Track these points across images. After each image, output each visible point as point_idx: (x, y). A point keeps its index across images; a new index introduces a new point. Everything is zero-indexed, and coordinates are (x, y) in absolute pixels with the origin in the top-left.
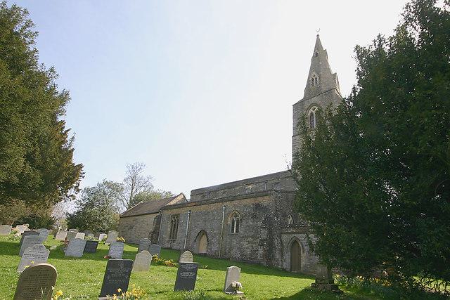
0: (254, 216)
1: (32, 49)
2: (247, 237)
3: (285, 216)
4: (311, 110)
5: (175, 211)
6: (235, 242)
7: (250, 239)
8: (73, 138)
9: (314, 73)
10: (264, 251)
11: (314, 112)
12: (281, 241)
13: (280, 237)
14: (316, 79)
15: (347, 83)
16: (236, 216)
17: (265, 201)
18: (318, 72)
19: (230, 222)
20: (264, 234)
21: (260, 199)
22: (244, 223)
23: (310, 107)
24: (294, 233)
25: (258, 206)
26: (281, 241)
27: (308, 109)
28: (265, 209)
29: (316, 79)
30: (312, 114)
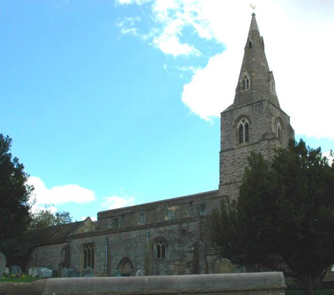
4: (241, 122)
5: (89, 240)
7: (177, 262)
11: (243, 125)
13: (205, 259)
14: (248, 81)
18: (250, 73)
22: (170, 248)
23: (241, 117)
27: (237, 121)
28: (191, 235)
29: (248, 81)
30: (241, 126)
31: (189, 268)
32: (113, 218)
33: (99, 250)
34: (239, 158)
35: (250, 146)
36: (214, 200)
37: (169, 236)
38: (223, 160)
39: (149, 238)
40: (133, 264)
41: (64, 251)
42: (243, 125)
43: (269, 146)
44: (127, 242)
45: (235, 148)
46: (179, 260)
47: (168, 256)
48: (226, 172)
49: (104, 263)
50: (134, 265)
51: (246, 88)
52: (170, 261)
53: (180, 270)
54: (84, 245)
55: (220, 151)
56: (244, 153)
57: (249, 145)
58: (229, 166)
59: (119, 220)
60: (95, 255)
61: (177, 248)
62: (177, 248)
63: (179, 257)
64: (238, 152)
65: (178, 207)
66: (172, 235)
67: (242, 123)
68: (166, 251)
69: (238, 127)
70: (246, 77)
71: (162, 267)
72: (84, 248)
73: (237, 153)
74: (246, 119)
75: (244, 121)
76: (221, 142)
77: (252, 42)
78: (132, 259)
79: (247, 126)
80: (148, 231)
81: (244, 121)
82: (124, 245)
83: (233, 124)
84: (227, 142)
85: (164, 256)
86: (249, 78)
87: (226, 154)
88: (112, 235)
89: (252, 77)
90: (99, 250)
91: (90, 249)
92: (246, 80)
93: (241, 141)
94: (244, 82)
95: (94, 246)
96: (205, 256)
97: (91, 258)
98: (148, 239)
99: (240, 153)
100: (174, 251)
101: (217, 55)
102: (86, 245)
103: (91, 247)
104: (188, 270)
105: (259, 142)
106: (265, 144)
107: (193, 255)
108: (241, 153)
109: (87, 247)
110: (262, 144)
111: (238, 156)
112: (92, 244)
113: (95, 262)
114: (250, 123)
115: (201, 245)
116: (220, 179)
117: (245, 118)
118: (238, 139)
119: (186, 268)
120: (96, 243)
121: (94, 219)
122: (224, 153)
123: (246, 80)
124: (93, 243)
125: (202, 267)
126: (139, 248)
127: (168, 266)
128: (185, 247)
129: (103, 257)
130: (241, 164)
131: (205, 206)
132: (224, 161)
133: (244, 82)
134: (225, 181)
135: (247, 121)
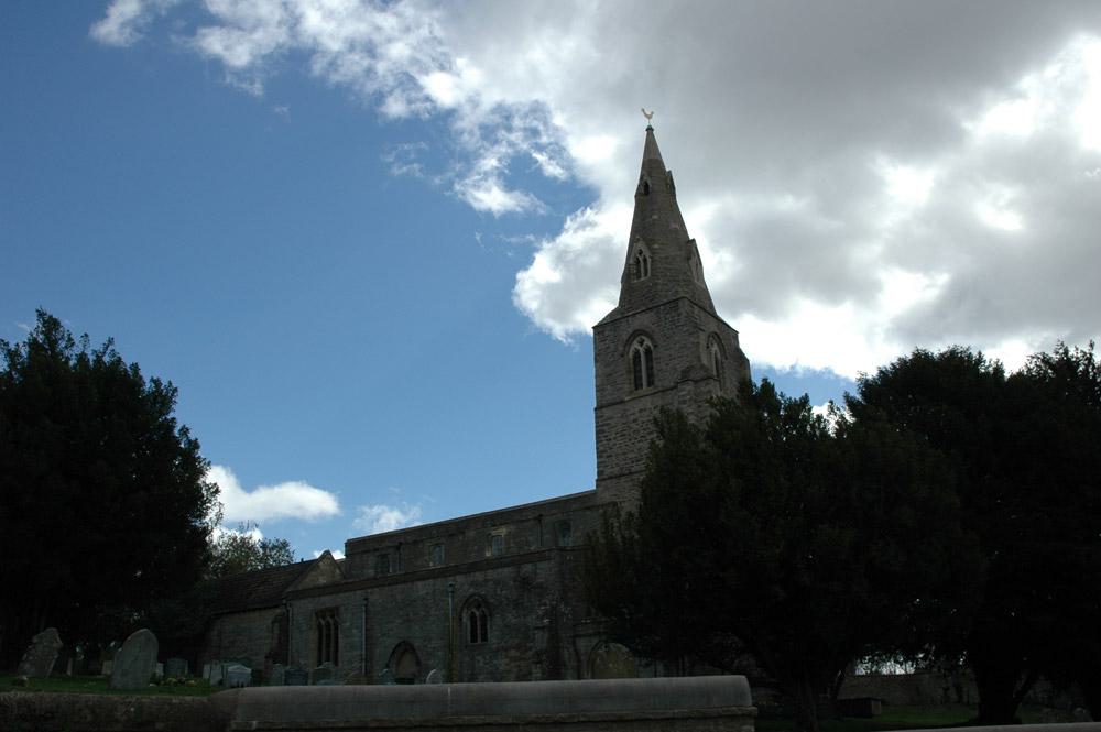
4: (635, 345)
5: (327, 601)
7: (513, 653)
11: (642, 350)
14: (645, 260)
18: (649, 243)
26: (575, 650)
27: (629, 342)
29: (645, 260)
30: (637, 353)
32: (377, 553)
34: (635, 421)
36: (588, 513)
42: (642, 350)
49: (359, 653)
60: (340, 636)
65: (512, 528)
69: (631, 354)
71: (481, 664)
75: (641, 343)
78: (417, 644)
79: (648, 352)
81: (641, 343)
83: (621, 349)
85: (484, 638)
86: (647, 254)
87: (607, 412)
89: (653, 252)
90: (348, 624)
91: (331, 621)
93: (638, 386)
94: (638, 262)
96: (575, 636)
103: (332, 616)
108: (640, 411)
112: (334, 611)
113: (340, 650)
115: (564, 613)
117: (643, 337)
118: (632, 381)
122: (604, 410)
123: (641, 259)
124: (337, 608)
126: (431, 618)
132: (605, 428)
135: (647, 342)
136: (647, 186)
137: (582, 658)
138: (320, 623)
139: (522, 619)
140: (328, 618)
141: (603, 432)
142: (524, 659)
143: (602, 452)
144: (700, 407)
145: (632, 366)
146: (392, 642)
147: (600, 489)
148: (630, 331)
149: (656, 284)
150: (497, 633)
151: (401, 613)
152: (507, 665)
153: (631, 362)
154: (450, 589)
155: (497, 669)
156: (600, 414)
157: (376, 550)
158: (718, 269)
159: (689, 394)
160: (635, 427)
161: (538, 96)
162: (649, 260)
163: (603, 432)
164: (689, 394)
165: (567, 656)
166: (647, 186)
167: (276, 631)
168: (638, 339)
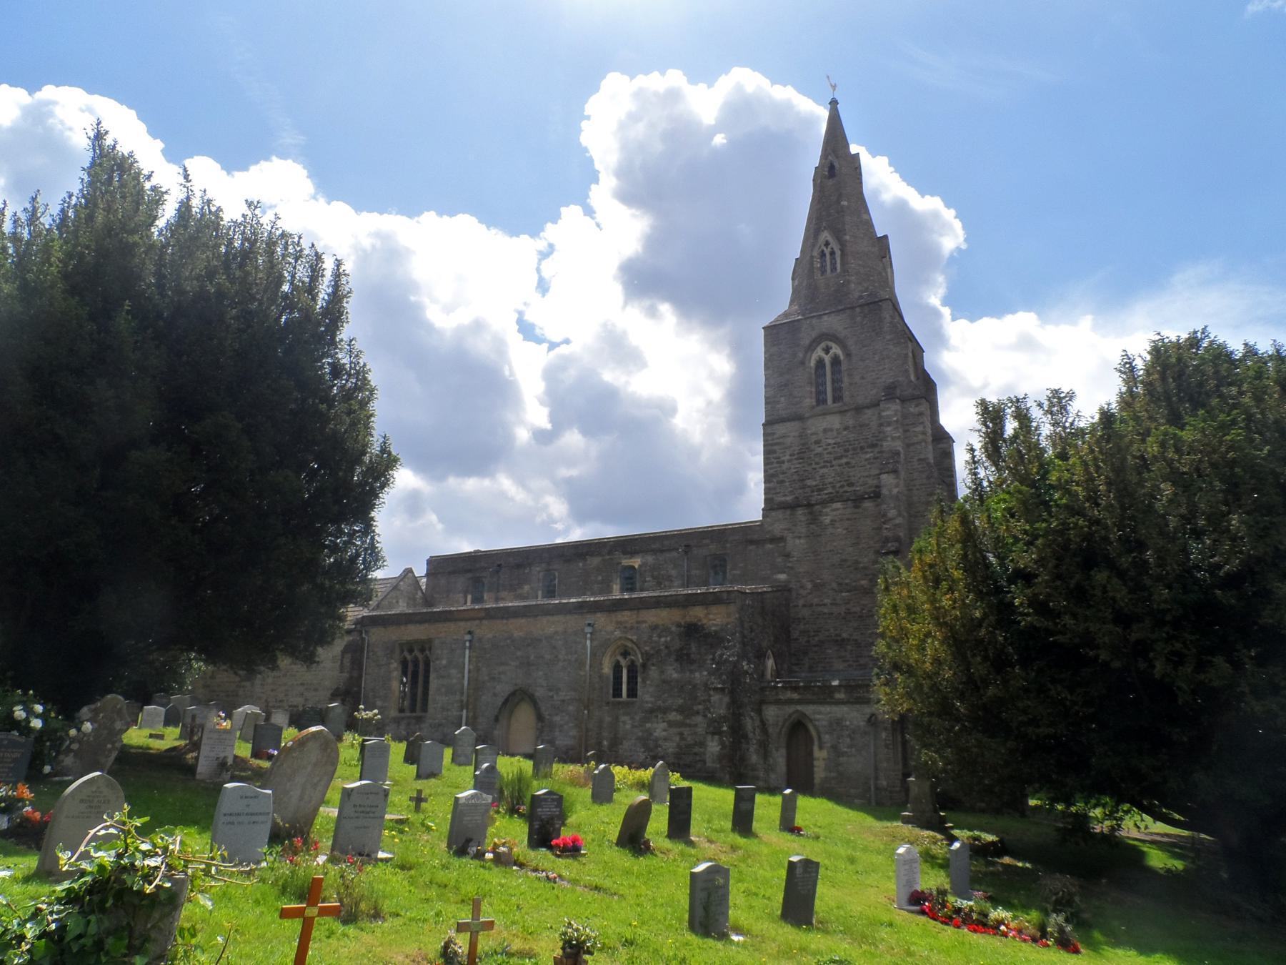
0: (683, 658)
1: (347, 289)
2: (665, 711)
3: (761, 656)
4: (819, 352)
5: (415, 632)
6: (626, 723)
7: (674, 716)
8: (257, 822)
9: (825, 235)
10: (722, 744)
11: (827, 359)
12: (762, 721)
13: (759, 712)
14: (832, 253)
15: (1148, 358)
16: (625, 654)
17: (715, 619)
18: (838, 234)
19: (607, 669)
20: (720, 705)
21: (697, 613)
22: (653, 672)
23: (822, 337)
24: (799, 702)
25: (692, 630)
26: (762, 721)
27: (811, 348)
28: (712, 640)
29: (832, 253)
30: (820, 363)
31: (716, 737)
32: (469, 575)
33: (444, 662)
34: (818, 442)
35: (849, 414)
36: (752, 547)
37: (651, 637)
38: (772, 445)
39: (592, 640)
40: (543, 709)
41: (348, 656)
42: (827, 359)
43: (904, 416)
44: (529, 645)
45: (807, 415)
46: (680, 710)
47: (647, 694)
48: (781, 477)
49: (458, 697)
50: (546, 714)
51: (829, 271)
52: (652, 711)
53: (682, 738)
54: (401, 645)
55: (762, 419)
56: (831, 430)
57: (846, 411)
58: (789, 461)
59: (486, 581)
60: (432, 676)
61: (675, 675)
62: (675, 675)
63: (681, 701)
64: (817, 426)
65: (650, 559)
66: (660, 637)
67: (822, 354)
68: (639, 679)
69: (813, 363)
70: (827, 244)
71: (628, 727)
72: (402, 651)
73: (813, 430)
74: (834, 345)
75: (827, 350)
76: (766, 398)
77: (836, 164)
78: (539, 693)
79: (836, 361)
80: (590, 618)
81: (827, 350)
82: (519, 653)
83: (801, 355)
84: (783, 399)
85: (632, 692)
86: (834, 245)
87: (781, 429)
88: (485, 622)
89: (843, 245)
90: (444, 662)
91: (420, 657)
92: (827, 251)
93: (821, 400)
94: (823, 254)
95: (430, 649)
96: (762, 702)
97: (421, 679)
98: (588, 642)
99: (821, 429)
100: (664, 682)
101: (633, 211)
102: (410, 646)
103: (422, 650)
104: (715, 743)
105: (878, 405)
106: (897, 411)
107: (726, 699)
108: (825, 431)
109: (411, 651)
110: (888, 409)
111: (814, 438)
112: (425, 646)
113: (431, 692)
114: (848, 355)
115: (747, 672)
116: (765, 494)
117: (830, 344)
118: (814, 395)
119: (709, 737)
120: (437, 642)
121: (420, 571)
122: (776, 426)
123: (827, 251)
124: (430, 641)
125: (751, 735)
126: (561, 664)
127: (648, 725)
128: (697, 675)
129: (454, 681)
130: (826, 457)
131: (725, 560)
132: (775, 448)
133: (823, 254)
134: (780, 499)
135: (836, 349)
136: (832, 167)
137: (770, 730)
138: (405, 658)
139: (688, 674)
140: (417, 653)
141: (775, 452)
142: (690, 726)
143: (773, 476)
144: (908, 431)
145: (813, 376)
146: (504, 689)
147: (768, 520)
148: (814, 334)
149: (849, 282)
150: (651, 689)
151: (519, 653)
152: (665, 730)
153: (813, 372)
154: (588, 630)
155: (651, 734)
156: (769, 430)
157: (470, 571)
158: (203, 742)
159: (896, 415)
160: (819, 450)
161: (280, 921)
162: (838, 253)
163: (775, 452)
164: (896, 415)
165: (749, 727)
166: (832, 167)
167: (347, 662)
168: (823, 345)
